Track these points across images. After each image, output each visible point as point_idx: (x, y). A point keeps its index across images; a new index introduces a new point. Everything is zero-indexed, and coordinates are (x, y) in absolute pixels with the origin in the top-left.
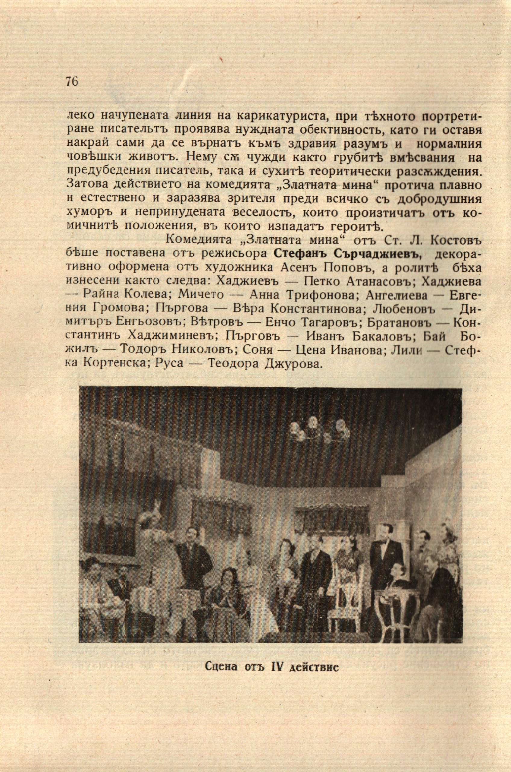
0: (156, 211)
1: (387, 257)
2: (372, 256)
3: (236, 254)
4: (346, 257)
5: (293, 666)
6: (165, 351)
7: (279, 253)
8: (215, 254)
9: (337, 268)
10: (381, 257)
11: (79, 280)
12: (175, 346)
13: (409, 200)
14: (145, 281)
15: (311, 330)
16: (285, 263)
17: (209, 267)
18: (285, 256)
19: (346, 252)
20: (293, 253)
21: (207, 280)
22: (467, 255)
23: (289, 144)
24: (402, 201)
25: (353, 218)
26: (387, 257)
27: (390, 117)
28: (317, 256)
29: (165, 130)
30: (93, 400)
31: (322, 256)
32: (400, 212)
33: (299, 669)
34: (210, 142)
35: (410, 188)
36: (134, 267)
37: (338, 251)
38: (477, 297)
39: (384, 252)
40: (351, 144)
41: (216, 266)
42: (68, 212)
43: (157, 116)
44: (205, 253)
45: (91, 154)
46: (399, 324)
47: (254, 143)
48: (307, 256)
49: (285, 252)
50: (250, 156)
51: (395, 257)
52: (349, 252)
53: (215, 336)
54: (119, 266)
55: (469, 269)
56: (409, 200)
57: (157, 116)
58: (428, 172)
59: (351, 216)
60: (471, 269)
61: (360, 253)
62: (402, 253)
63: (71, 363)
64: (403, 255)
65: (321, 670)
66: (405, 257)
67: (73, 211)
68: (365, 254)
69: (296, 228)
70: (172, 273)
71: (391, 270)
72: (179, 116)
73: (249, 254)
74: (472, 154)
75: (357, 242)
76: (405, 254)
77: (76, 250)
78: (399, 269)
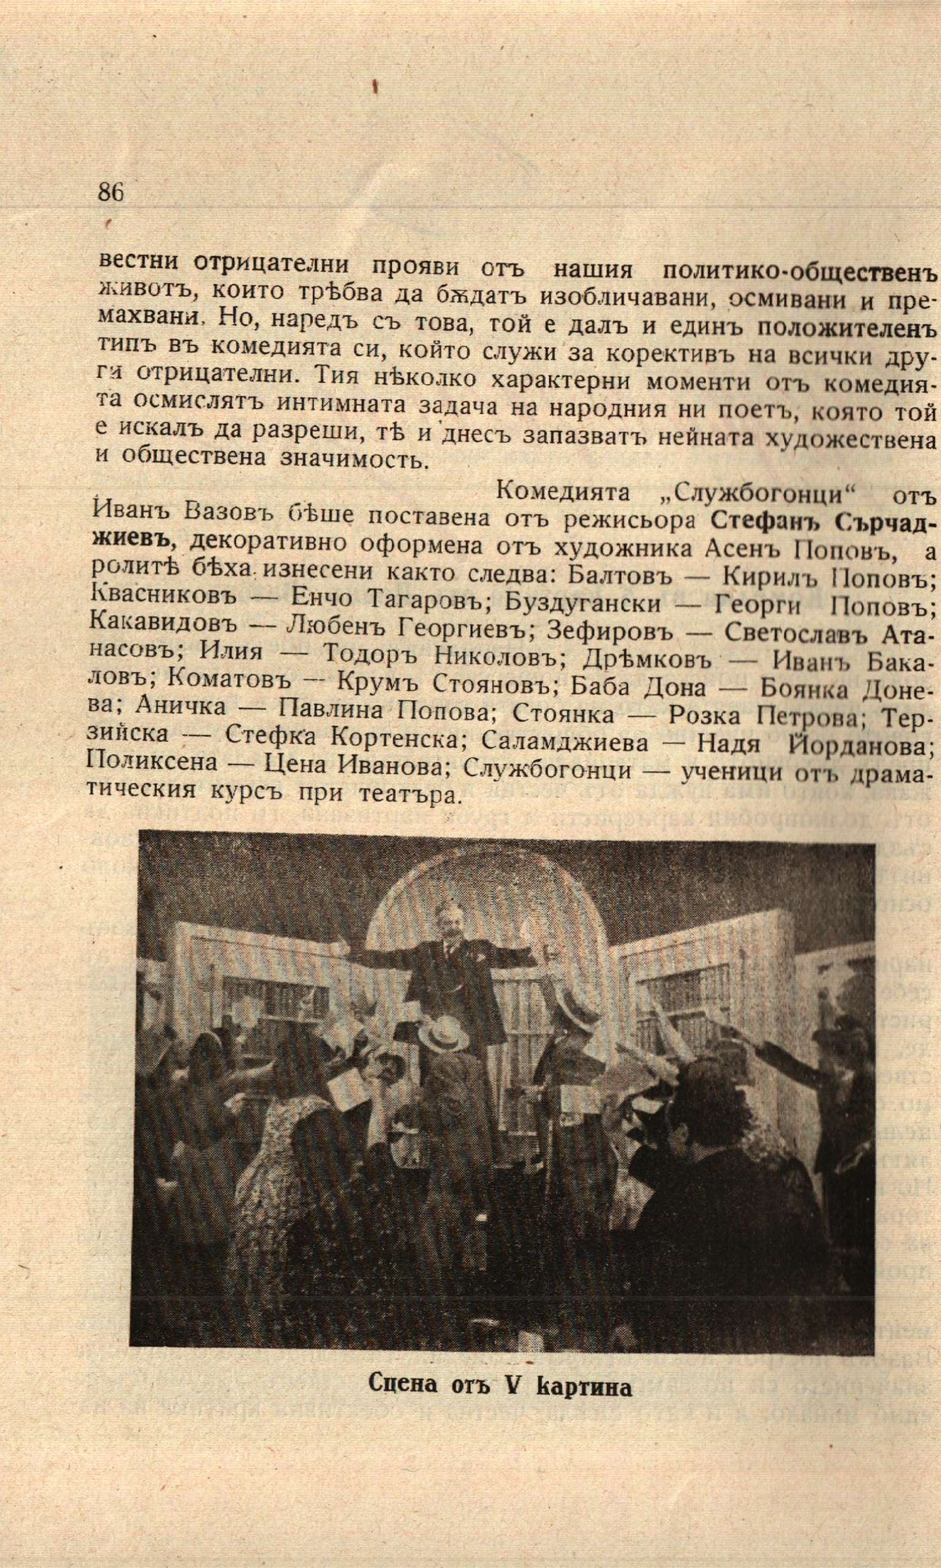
1: (108, 543)
4: (859, 529)
7: (721, 519)
8: (593, 520)
9: (821, 552)
11: (291, 570)
12: (704, 738)
16: (713, 541)
17: (773, 439)
18: (735, 526)
19: (860, 520)
20: (752, 518)
22: (255, 542)
28: (800, 528)
30: (170, 867)
32: (633, 297)
35: (469, 1392)
36: (414, 547)
37: (683, 486)
38: (925, 695)
39: (102, 533)
41: (577, 546)
42: (768, 439)
44: (571, 521)
45: (625, 655)
47: (558, 381)
49: (735, 518)
50: (836, 355)
52: (867, 520)
58: (460, 296)
61: (888, 520)
62: (137, 536)
63: (444, 742)
65: (884, 279)
66: (143, 544)
69: (731, 748)
70: (490, 559)
73: (661, 522)
76: (144, 539)
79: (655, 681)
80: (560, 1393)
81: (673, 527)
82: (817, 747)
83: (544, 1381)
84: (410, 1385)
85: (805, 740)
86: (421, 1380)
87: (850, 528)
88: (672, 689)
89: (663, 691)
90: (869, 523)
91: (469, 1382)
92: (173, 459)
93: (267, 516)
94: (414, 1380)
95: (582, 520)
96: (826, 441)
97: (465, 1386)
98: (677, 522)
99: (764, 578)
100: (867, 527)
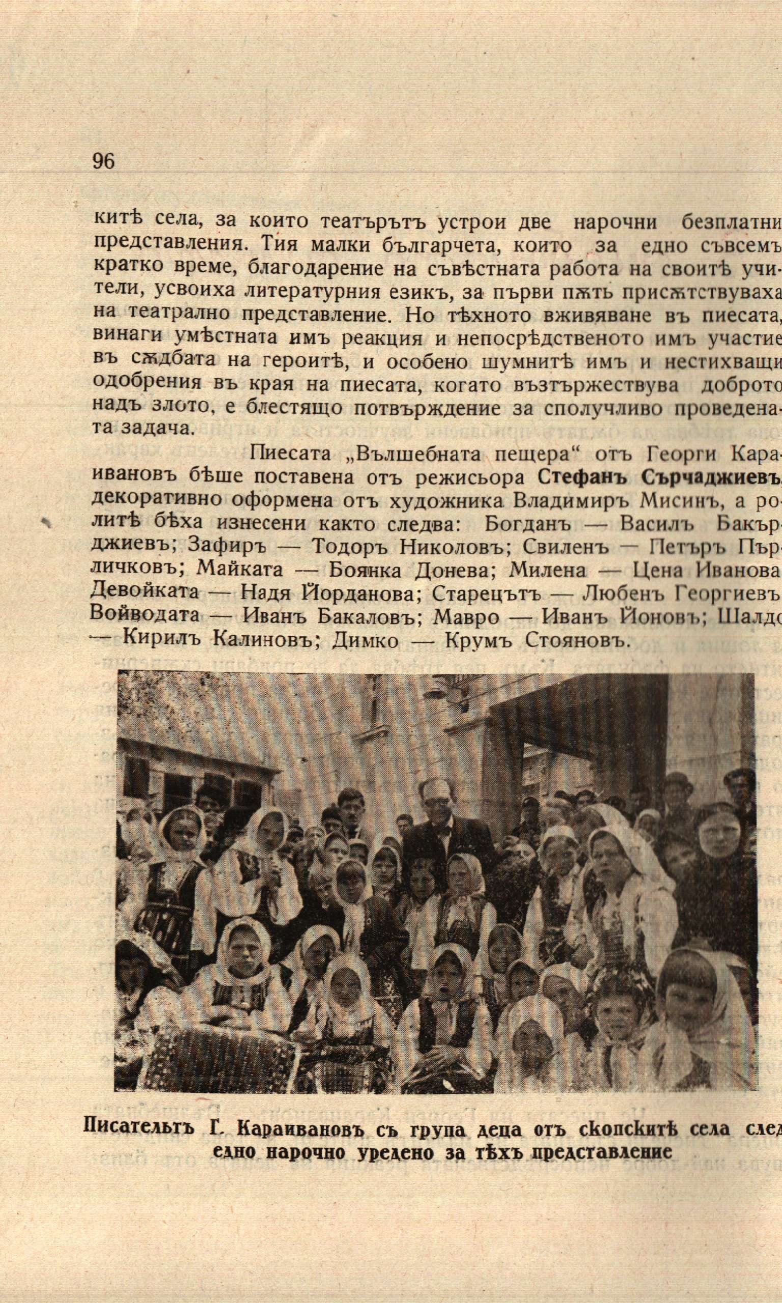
0: (106, 240)
2: (705, 480)
3: (475, 479)
4: (661, 482)
5: (483, 1128)
6: (511, 644)
7: (546, 476)
8: (439, 479)
10: (719, 482)
13: (720, 386)
14: (351, 525)
15: (252, 605)
18: (556, 481)
19: (661, 475)
20: (570, 476)
21: (454, 523)
23: (463, 293)
24: (709, 387)
25: (687, 416)
26: (730, 482)
27: (418, 456)
28: (610, 481)
29: (608, 295)
31: (619, 482)
33: (406, 1155)
34: (525, 292)
37: (649, 473)
40: (301, 292)
41: (408, 500)
42: (392, 503)
43: (520, 270)
46: (374, 595)
48: (592, 482)
51: (743, 483)
53: (702, 619)
54: (250, 499)
55: (181, 522)
56: (720, 386)
57: (131, 1128)
58: (583, 293)
59: (683, 414)
60: (186, 522)
61: (685, 475)
62: (755, 476)
64: (757, 480)
67: (401, 502)
68: (694, 477)
71: (751, 503)
72: (340, 1154)
73: (495, 479)
74: (233, 354)
75: (349, 503)
77: (206, 470)
78: (422, 480)
79: (424, 566)
80: (286, 1157)
81: (505, 483)
82: (326, 595)
83: (639, 1125)
84: (411, 1154)
85: (316, 589)
86: (275, 1149)
87: (653, 482)
88: (438, 572)
89: (431, 574)
90: (669, 477)
91: (548, 1127)
92: (329, 411)
93: (172, 477)
94: (414, 1150)
95: (430, 479)
96: (428, 410)
97: (545, 1131)
98: (508, 479)
99: (641, 293)
100: (667, 481)
